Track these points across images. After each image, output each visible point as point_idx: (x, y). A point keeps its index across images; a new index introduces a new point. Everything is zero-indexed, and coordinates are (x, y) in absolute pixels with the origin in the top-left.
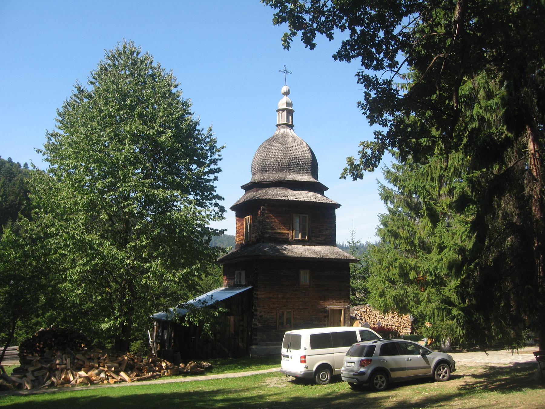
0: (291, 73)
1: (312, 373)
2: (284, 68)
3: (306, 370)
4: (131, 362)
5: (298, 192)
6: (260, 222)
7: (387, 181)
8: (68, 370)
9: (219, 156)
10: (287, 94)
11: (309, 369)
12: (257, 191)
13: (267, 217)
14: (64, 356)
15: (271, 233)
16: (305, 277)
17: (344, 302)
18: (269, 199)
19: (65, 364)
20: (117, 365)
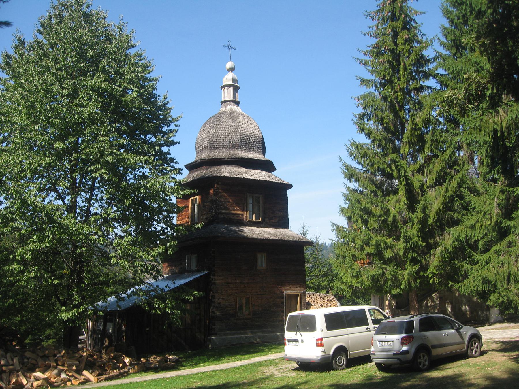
0: (235, 49)
1: (329, 357)
3: (324, 354)
4: (91, 359)
5: (251, 170)
6: (212, 202)
7: (351, 159)
8: (18, 371)
9: (177, 126)
10: (232, 70)
12: (207, 169)
13: (221, 197)
14: (8, 355)
15: (226, 213)
16: (262, 261)
17: (300, 287)
18: (224, 177)
19: (12, 365)
20: (77, 362)
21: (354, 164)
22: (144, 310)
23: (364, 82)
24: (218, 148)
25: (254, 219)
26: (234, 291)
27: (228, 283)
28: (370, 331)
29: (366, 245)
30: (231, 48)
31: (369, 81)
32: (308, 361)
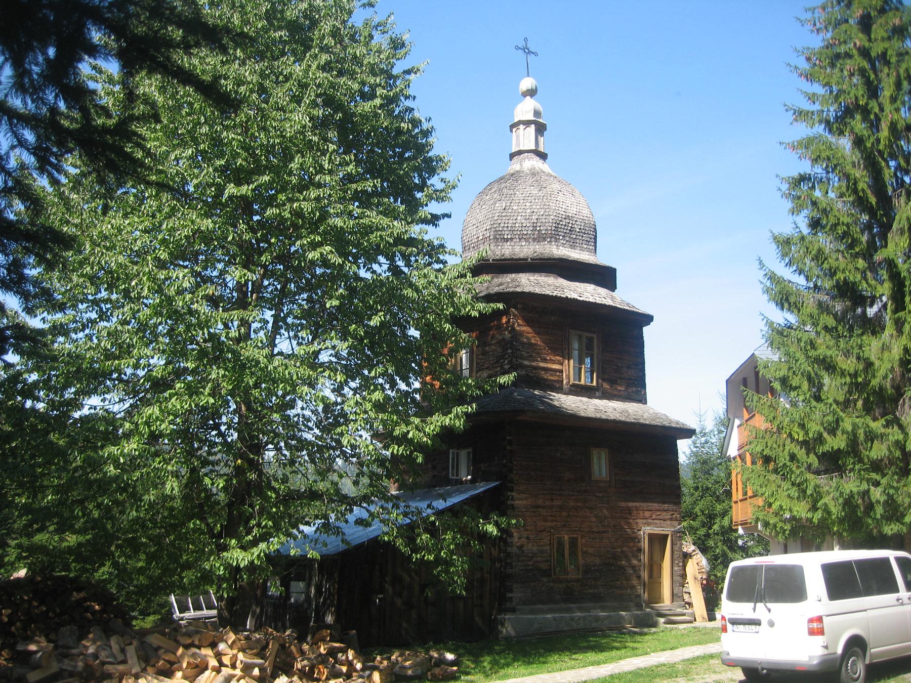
0: (536, 54)
3: (826, 652)
5: (577, 284)
7: (783, 264)
10: (532, 93)
11: (831, 651)
16: (600, 465)
21: (787, 273)
22: (395, 550)
23: (801, 115)
24: (511, 239)
25: (582, 382)
26: (549, 524)
27: (538, 507)
28: (902, 604)
29: (829, 433)
30: (530, 52)
31: (813, 113)
32: (788, 668)
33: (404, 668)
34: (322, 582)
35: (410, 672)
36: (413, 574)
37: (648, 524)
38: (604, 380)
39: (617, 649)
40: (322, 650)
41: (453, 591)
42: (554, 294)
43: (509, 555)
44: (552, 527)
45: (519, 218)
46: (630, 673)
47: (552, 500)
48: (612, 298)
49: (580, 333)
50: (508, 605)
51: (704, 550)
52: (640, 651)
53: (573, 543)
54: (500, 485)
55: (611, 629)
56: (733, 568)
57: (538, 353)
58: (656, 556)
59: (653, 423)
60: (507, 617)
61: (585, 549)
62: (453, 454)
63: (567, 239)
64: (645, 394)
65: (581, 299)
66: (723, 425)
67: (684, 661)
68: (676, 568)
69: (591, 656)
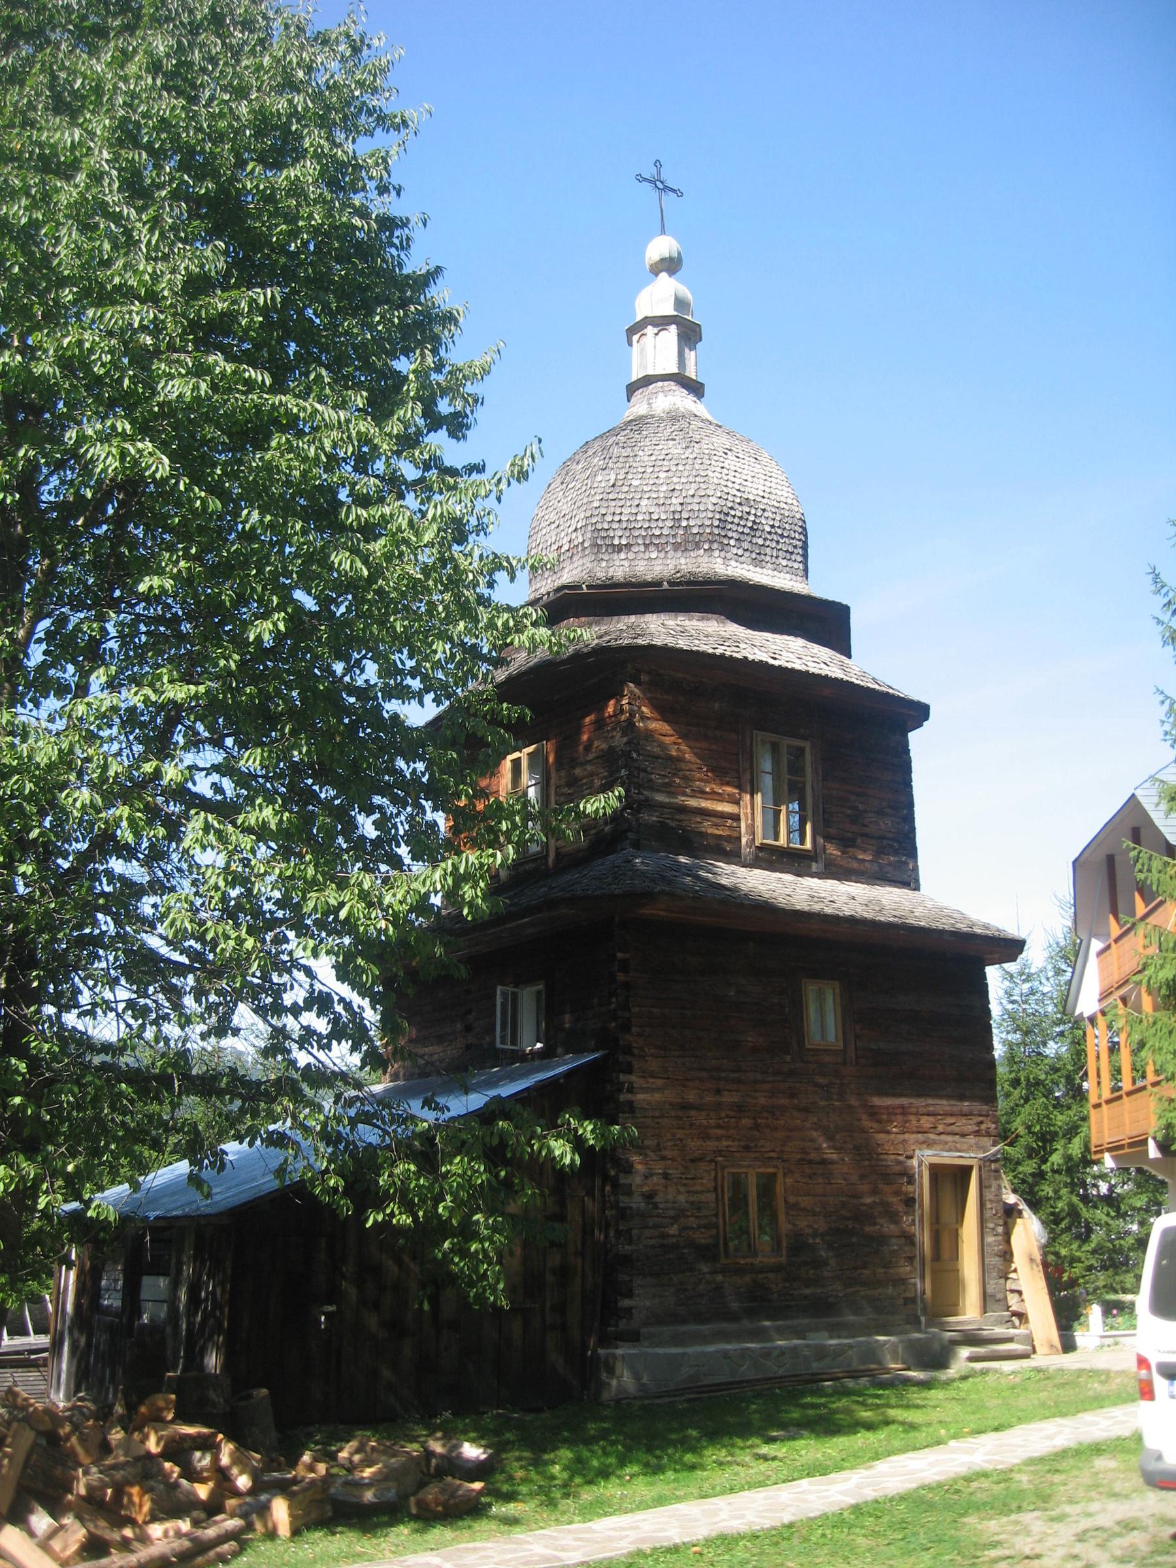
2: (654, 171)
10: (671, 265)
16: (824, 1017)
25: (782, 841)
26: (711, 1144)
27: (686, 1107)
30: (667, 189)
33: (360, 1485)
34: (200, 1276)
35: (369, 1496)
36: (406, 1259)
37: (929, 1144)
38: (828, 838)
39: (870, 1427)
40: (153, 1445)
41: (481, 1298)
42: (718, 652)
43: (624, 1214)
44: (719, 1152)
45: (644, 503)
46: (902, 1498)
47: (718, 1092)
48: (842, 667)
49: (774, 737)
50: (623, 1325)
51: (1035, 1205)
52: (921, 1436)
53: (767, 1189)
54: (604, 1057)
55: (855, 1375)
56: (1166, 1233)
57: (686, 779)
58: (948, 1214)
59: (934, 925)
60: (619, 1352)
61: (792, 1199)
62: (504, 994)
63: (746, 545)
64: (916, 869)
65: (776, 663)
66: (1065, 958)
67: (1031, 1462)
68: (990, 1239)
69: (808, 1449)
